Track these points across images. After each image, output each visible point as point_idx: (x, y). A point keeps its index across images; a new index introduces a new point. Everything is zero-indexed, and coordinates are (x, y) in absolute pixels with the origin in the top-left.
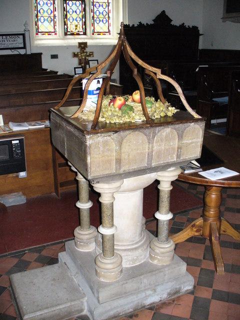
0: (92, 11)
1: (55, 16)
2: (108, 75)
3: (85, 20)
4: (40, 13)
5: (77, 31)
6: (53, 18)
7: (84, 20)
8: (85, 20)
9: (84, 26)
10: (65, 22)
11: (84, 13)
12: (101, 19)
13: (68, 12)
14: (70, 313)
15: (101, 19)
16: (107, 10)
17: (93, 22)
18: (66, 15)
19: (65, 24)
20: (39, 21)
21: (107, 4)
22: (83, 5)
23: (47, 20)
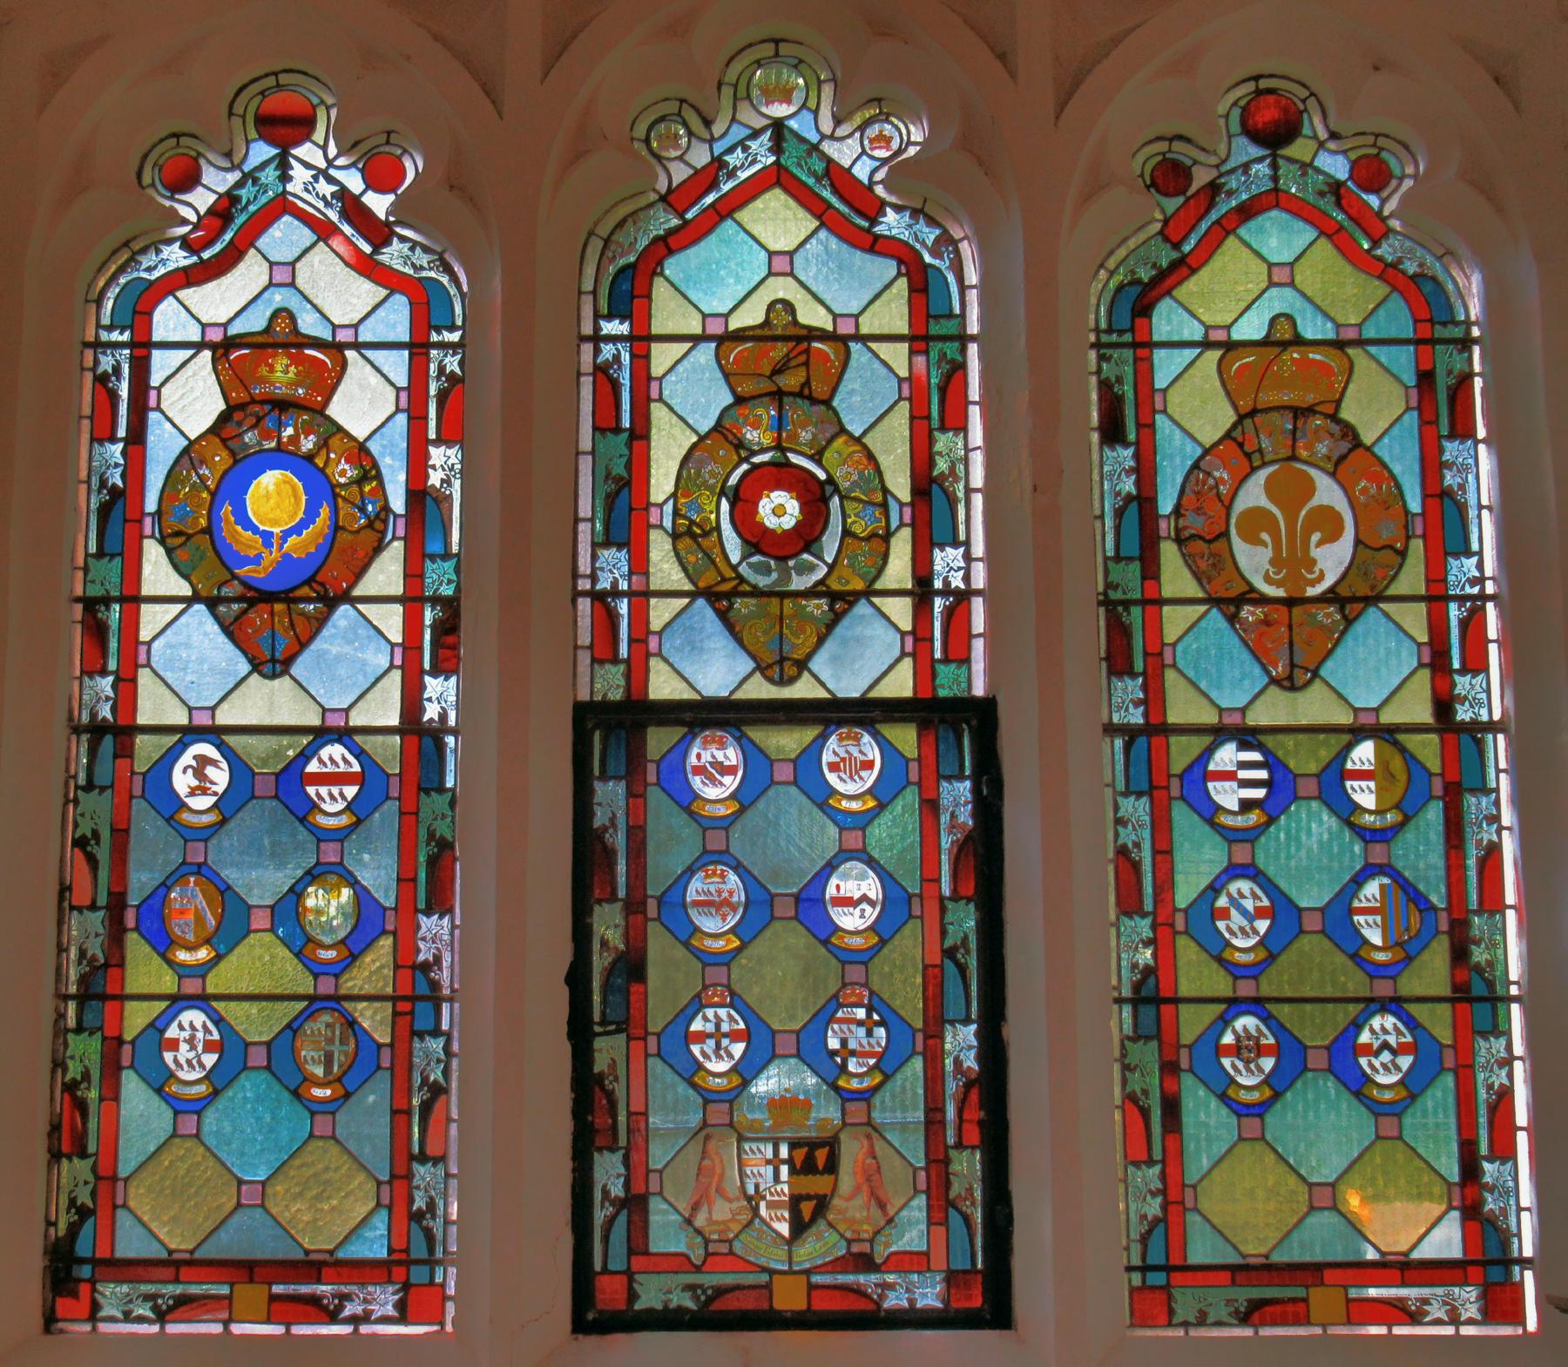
0: (1136, 884)
1: (415, 994)
2: (1181, 522)
3: (989, 808)
4: (164, 944)
5: (819, 1247)
6: (375, 1021)
7: (962, 1041)
8: (989, 808)
9: (968, 1166)
10: (587, 1088)
11: (965, 921)
12: (1316, 1029)
13: (673, 900)
14: (864, 1171)
15: (1316, 1029)
16: (1421, 853)
17: (1140, 837)
18: (632, 966)
19: (594, 1115)
20: (131, 1083)
21: (1428, 749)
22: (958, 795)
23: (279, 1058)
